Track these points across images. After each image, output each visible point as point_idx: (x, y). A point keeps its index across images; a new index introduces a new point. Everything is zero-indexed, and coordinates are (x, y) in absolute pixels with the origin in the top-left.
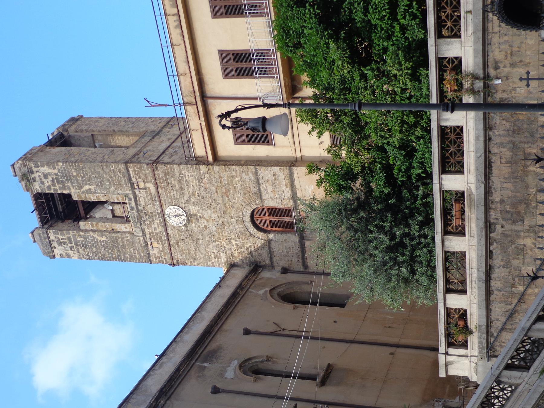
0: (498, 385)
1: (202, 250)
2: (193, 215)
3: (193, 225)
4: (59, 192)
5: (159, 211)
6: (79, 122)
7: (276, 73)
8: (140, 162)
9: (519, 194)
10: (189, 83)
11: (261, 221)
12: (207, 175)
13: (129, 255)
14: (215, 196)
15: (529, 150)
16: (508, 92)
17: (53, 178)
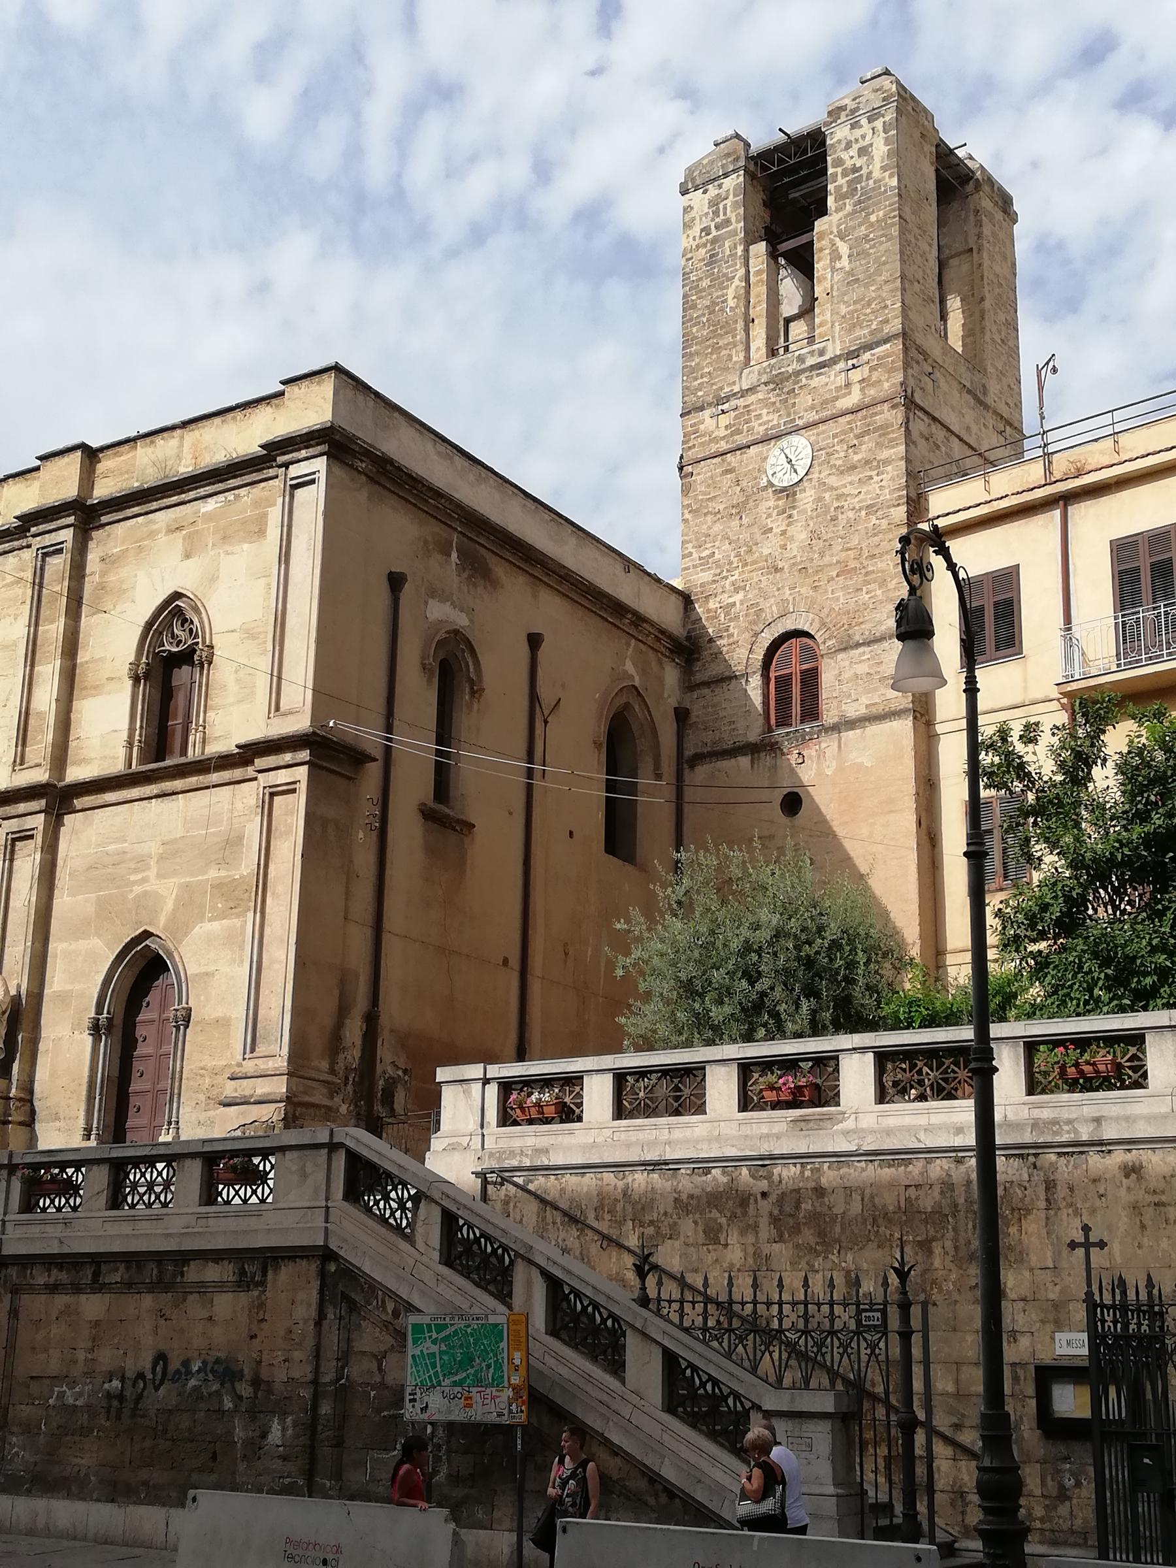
0: (410, 1197)
1: (717, 527)
2: (794, 501)
3: (771, 503)
4: (830, 187)
5: (800, 423)
6: (999, 215)
7: (1130, 663)
8: (906, 365)
9: (838, 1229)
10: (1100, 462)
11: (788, 655)
12: (884, 522)
13: (697, 364)
14: (837, 546)
15: (937, 1250)
16: (1069, 1200)
17: (861, 168)
